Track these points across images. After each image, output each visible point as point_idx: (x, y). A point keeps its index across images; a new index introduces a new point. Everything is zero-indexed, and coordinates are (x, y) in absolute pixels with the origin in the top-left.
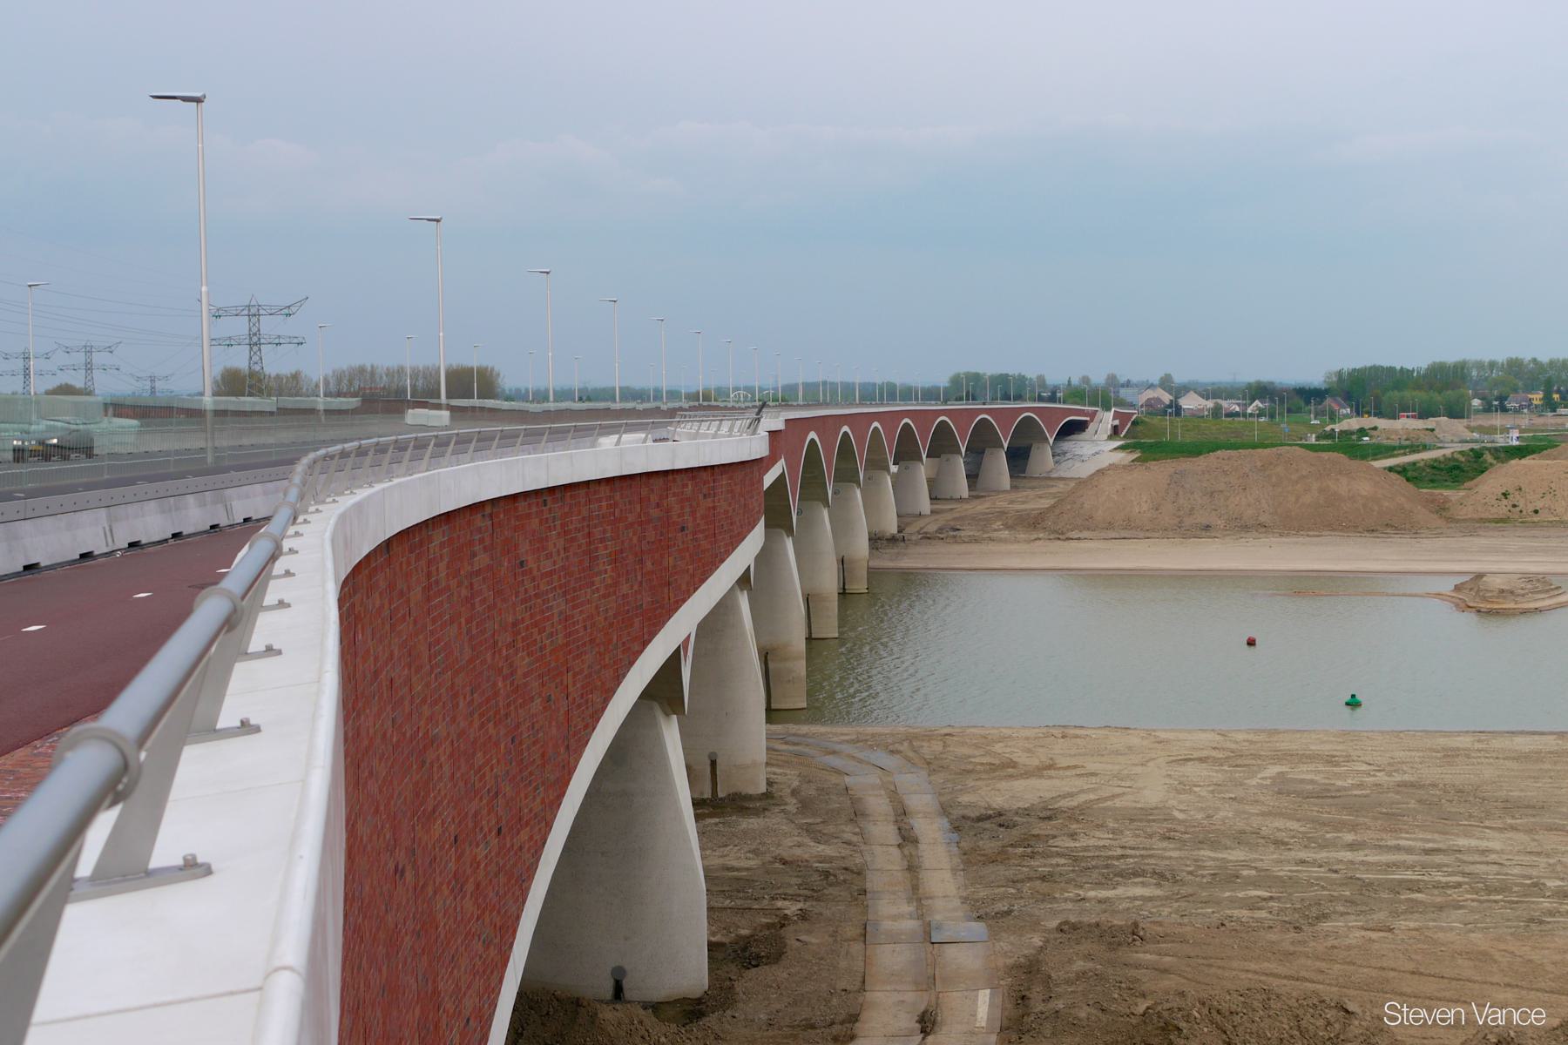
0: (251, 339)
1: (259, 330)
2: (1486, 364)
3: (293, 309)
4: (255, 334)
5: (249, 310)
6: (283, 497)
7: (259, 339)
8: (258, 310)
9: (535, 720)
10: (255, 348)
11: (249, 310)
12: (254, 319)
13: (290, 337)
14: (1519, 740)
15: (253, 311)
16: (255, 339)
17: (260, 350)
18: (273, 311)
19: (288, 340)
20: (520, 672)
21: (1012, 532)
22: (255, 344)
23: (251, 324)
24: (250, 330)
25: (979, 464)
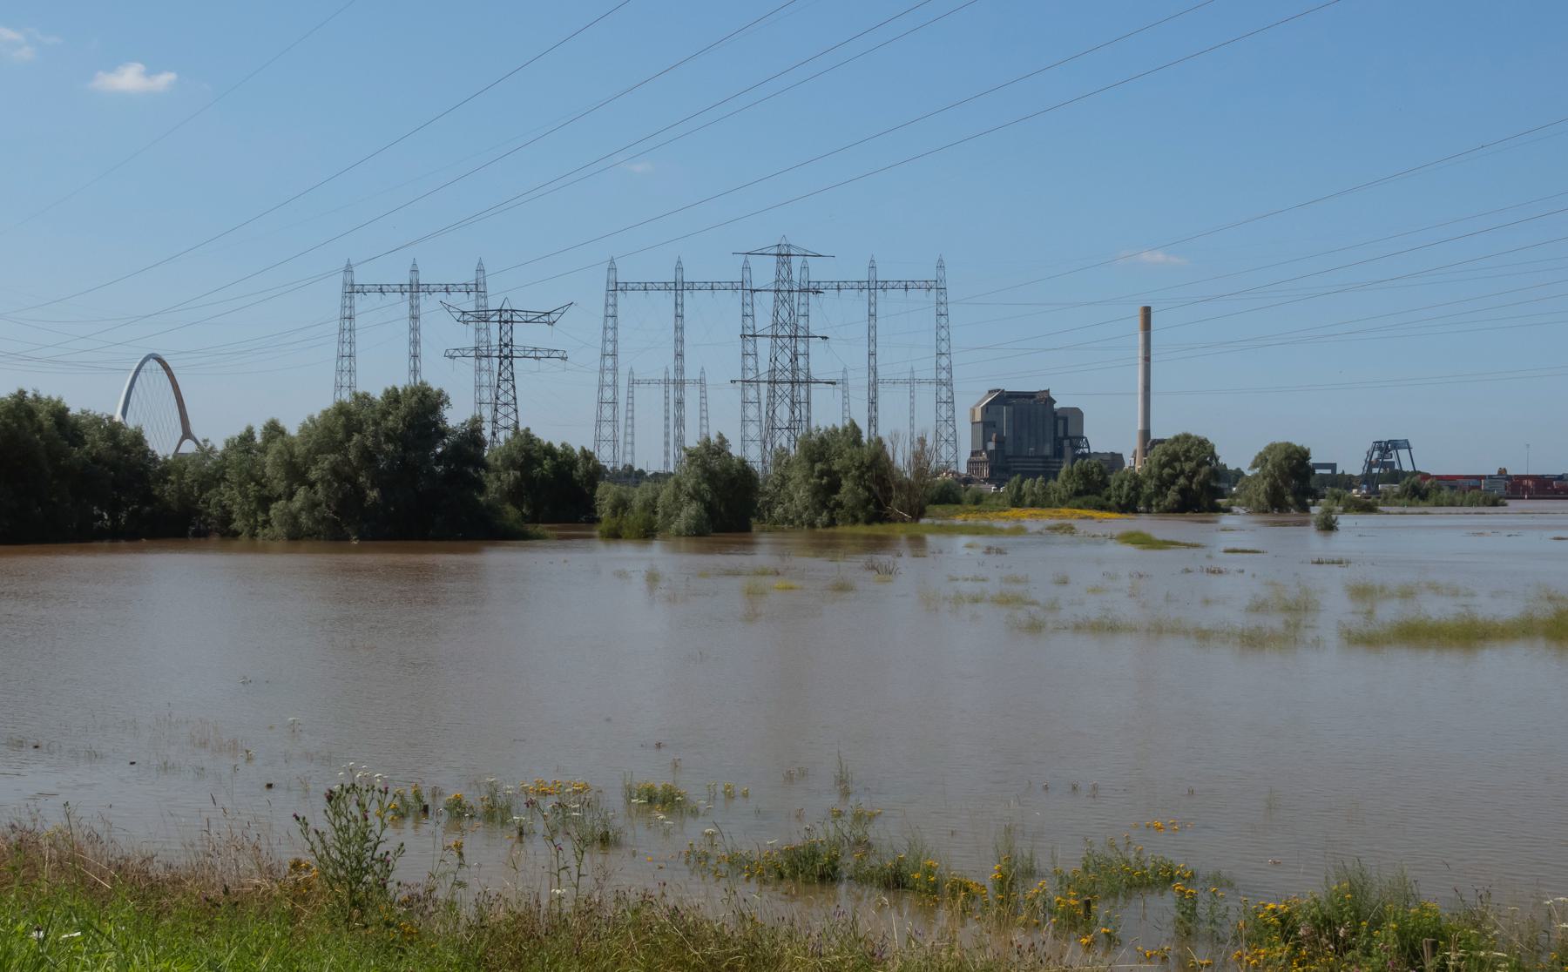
0: (501, 351)
1: (511, 340)
2: (840, 524)
3: (554, 317)
4: (506, 345)
5: (501, 316)
6: (1346, 864)
7: (511, 351)
8: (512, 316)
9: (244, 930)
10: (506, 362)
11: (501, 316)
12: (506, 327)
13: (549, 350)
14: (1417, 511)
15: (506, 316)
16: (506, 351)
17: (511, 363)
18: (529, 319)
19: (522, 353)
20: (345, 933)
21: (1262, 498)
22: (506, 357)
23: (503, 333)
24: (501, 340)
25: (1158, 542)
